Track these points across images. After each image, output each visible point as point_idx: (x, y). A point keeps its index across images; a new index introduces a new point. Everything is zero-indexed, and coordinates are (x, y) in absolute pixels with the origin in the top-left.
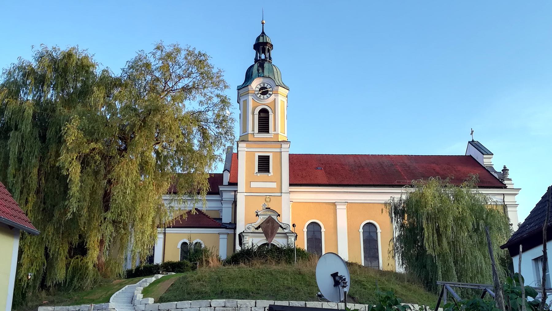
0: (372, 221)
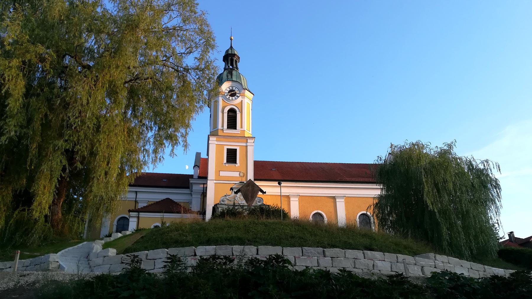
0: (320, 212)
